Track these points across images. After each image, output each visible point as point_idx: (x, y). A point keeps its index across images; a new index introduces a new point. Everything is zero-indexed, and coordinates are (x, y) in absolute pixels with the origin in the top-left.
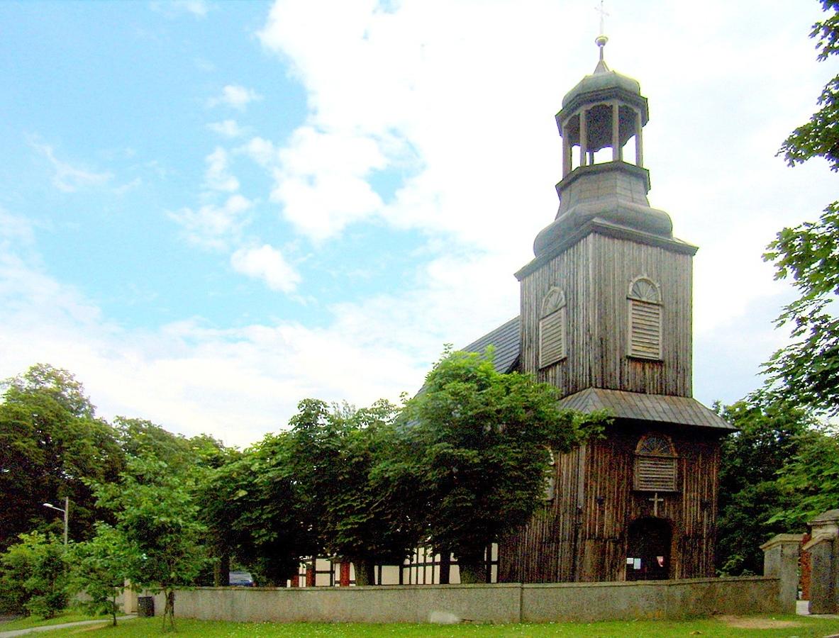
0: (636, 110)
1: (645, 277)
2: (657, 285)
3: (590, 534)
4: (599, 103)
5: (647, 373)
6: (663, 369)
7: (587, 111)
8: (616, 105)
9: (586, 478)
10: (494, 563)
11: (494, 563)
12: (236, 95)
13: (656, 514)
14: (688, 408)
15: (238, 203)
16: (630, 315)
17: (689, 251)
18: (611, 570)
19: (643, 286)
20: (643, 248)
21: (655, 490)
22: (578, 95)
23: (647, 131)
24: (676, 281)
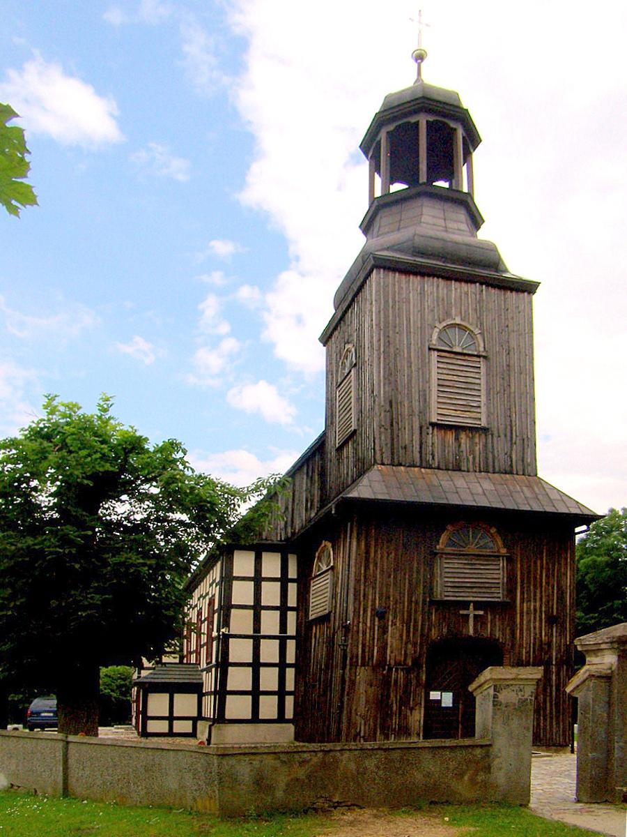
1: (458, 321)
2: (477, 331)
3: (363, 657)
5: (463, 446)
6: (490, 440)
7: (388, 132)
9: (358, 581)
10: (290, 693)
11: (290, 693)
12: (223, 248)
13: (471, 632)
14: (525, 489)
15: (230, 345)
16: (434, 371)
17: (528, 288)
18: (400, 708)
19: (455, 335)
20: (454, 285)
21: (471, 599)
24: (507, 326)
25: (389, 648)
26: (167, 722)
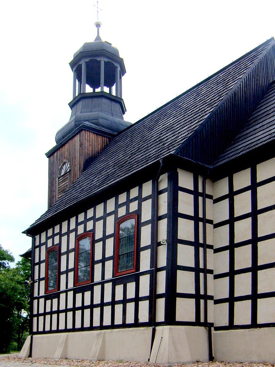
0: (116, 64)
4: (92, 58)
8: (103, 60)
22: (80, 52)
23: (125, 79)
25: (135, 260)
26: (193, 274)
